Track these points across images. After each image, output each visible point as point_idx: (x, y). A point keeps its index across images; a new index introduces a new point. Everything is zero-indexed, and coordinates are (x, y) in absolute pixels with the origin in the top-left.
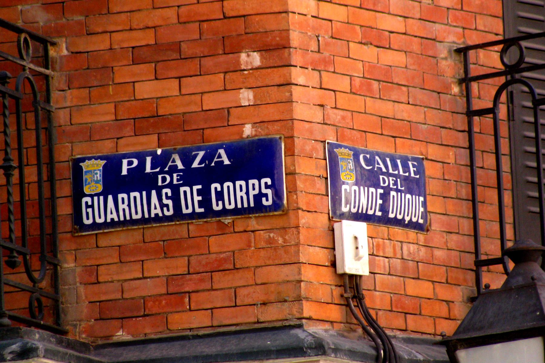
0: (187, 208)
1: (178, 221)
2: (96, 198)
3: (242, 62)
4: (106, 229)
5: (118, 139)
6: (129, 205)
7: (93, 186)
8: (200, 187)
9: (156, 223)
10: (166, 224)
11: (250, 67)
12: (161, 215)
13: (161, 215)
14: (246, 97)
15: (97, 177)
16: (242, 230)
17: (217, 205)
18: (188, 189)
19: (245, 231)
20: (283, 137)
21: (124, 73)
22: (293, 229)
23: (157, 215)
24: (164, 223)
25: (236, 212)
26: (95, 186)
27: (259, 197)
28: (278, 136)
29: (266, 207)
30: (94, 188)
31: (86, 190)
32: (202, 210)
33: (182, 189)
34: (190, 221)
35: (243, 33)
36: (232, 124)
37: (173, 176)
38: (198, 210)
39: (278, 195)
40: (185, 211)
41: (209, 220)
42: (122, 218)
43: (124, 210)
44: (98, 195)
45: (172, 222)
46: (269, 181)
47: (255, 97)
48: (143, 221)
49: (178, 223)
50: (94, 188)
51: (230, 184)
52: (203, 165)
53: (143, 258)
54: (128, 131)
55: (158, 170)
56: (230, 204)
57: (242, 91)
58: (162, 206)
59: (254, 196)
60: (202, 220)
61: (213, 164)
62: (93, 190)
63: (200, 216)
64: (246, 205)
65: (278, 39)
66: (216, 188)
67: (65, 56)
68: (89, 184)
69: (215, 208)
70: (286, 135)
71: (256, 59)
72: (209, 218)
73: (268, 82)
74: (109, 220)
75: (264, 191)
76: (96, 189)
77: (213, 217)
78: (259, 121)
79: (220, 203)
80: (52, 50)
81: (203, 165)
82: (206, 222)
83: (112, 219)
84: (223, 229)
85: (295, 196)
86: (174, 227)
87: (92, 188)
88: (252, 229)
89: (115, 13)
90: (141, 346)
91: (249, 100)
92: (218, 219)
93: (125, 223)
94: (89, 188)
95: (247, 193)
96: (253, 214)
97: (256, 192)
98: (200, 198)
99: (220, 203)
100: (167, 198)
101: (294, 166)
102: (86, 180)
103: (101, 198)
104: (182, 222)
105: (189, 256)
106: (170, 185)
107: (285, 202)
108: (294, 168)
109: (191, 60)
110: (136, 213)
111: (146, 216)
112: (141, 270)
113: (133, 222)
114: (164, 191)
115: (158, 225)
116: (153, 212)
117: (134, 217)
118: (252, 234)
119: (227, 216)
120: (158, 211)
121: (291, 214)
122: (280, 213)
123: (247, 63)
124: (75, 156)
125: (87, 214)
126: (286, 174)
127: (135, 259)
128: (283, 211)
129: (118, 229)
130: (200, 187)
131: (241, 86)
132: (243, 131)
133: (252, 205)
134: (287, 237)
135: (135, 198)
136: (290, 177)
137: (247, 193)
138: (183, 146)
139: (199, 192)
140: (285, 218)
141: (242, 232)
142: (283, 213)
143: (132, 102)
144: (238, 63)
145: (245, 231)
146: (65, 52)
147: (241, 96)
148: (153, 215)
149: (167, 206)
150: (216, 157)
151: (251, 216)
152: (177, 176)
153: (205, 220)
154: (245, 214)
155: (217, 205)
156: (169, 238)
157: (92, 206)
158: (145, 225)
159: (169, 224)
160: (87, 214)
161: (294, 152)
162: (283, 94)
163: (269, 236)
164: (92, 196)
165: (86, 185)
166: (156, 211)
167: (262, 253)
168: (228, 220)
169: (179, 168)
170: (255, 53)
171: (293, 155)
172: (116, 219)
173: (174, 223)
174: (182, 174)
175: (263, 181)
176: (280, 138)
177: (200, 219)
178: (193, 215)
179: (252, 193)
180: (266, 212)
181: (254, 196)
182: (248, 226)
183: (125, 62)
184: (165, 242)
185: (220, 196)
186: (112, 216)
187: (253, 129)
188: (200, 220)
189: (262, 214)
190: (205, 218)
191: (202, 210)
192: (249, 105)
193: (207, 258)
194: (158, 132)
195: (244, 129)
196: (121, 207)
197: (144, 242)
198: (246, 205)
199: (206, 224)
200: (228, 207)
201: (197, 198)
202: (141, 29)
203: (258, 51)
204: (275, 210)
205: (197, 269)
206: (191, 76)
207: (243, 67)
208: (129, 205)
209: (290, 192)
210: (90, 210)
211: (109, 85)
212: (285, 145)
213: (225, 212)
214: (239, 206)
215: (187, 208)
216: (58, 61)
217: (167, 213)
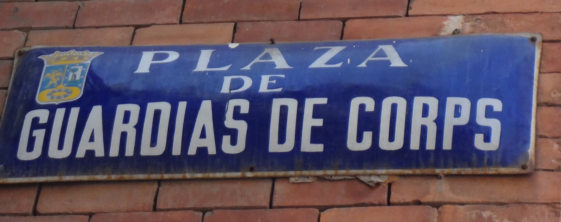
0: (282, 139)
1: (252, 170)
2: (60, 113)
4: (67, 174)
5: (137, 27)
6: (139, 127)
7: (60, 91)
8: (323, 101)
10: (219, 175)
12: (212, 151)
13: (212, 151)
15: (75, 76)
16: (409, 198)
17: (359, 139)
18: (292, 104)
19: (418, 203)
20: (539, 38)
22: (544, 207)
23: (202, 151)
24: (214, 171)
25: (404, 158)
26: (66, 91)
27: (464, 134)
29: (480, 153)
30: (57, 94)
31: (42, 98)
32: (319, 148)
33: (277, 104)
34: (281, 173)
36: (418, 13)
37: (260, 79)
38: (307, 146)
40: (274, 146)
41: (331, 172)
42: (114, 152)
43: (124, 135)
44: (68, 106)
45: (238, 171)
46: (497, 105)
49: (249, 174)
52: (339, 65)
56: (391, 138)
58: (220, 130)
59: (457, 129)
60: (313, 173)
61: (363, 65)
62: (59, 98)
63: (312, 161)
64: (431, 145)
68: (52, 86)
69: (352, 144)
72: (330, 168)
74: (80, 154)
75: (482, 120)
76: (65, 96)
77: (342, 167)
78: (483, 11)
79: (368, 136)
81: (339, 65)
82: (320, 178)
86: (237, 186)
87: (57, 94)
88: (437, 199)
92: (353, 172)
93: (121, 162)
95: (440, 122)
96: (446, 166)
97: (464, 120)
98: (319, 122)
99: (368, 136)
102: (47, 81)
103: (75, 112)
106: (252, 96)
107: (531, 150)
110: (154, 142)
111: (176, 150)
113: (140, 162)
117: (146, 150)
120: (210, 144)
122: (516, 170)
124: (30, 46)
126: (538, 105)
128: (524, 167)
129: (99, 177)
130: (323, 101)
132: (442, 26)
133: (447, 144)
135: (157, 114)
137: (440, 122)
139: (318, 112)
141: (407, 204)
142: (523, 172)
145: (418, 203)
148: (192, 151)
149: (233, 133)
150: (374, 54)
151: (438, 171)
152: (271, 79)
153: (320, 173)
154: (427, 166)
155: (359, 139)
156: (219, 205)
157: (48, 127)
158: (168, 172)
159: (229, 175)
163: (480, 216)
164: (52, 109)
165: (42, 90)
166: (203, 140)
168: (380, 175)
169: (278, 67)
172: (100, 152)
173: (238, 174)
174: (283, 76)
175: (482, 103)
176: (533, 40)
178: (295, 159)
179: (450, 122)
180: (480, 165)
181: (457, 129)
182: (427, 193)
184: (208, 214)
185: (369, 122)
187: (468, 24)
188: (306, 173)
190: (320, 168)
191: (319, 148)
194: (235, 18)
195: (445, 23)
196: (118, 126)
198: (431, 145)
199: (319, 185)
200: (384, 144)
201: (310, 122)
204: (504, 164)
208: (139, 127)
209: (541, 137)
210: (40, 134)
212: (542, 54)
213: (374, 157)
214: (415, 145)
215: (282, 139)
217: (227, 148)
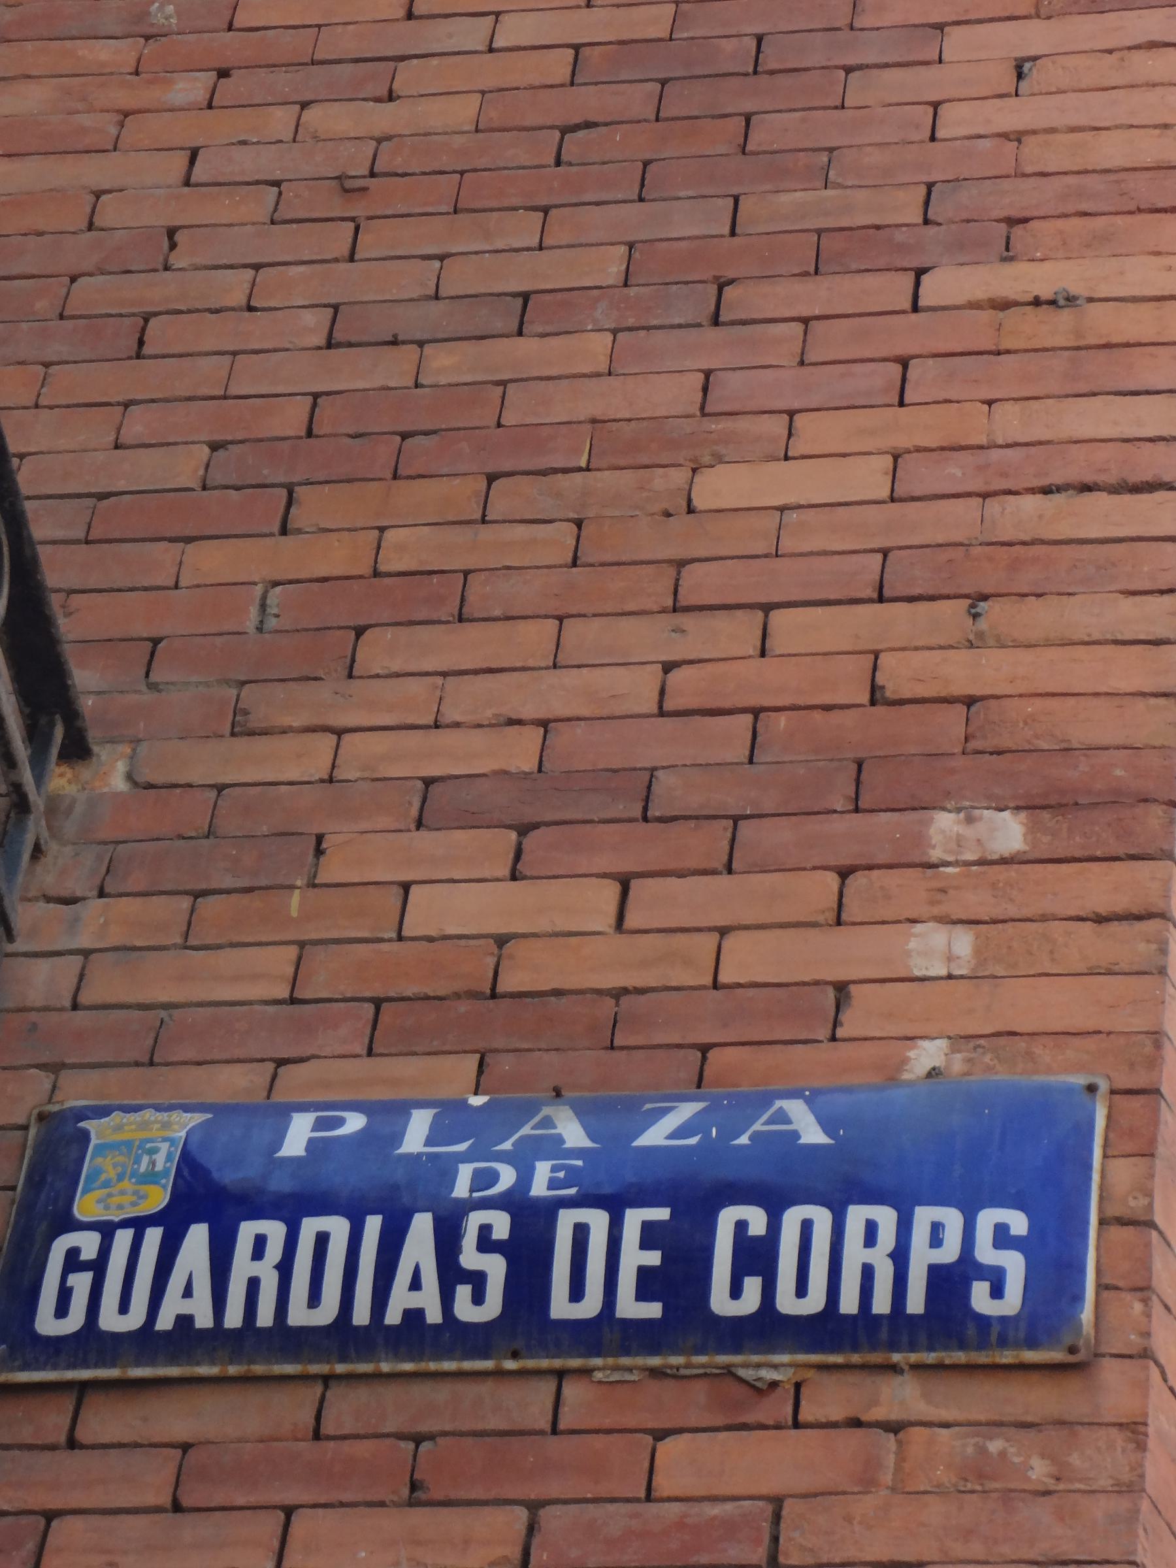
0: (577, 1292)
1: (515, 1355)
2: (123, 1239)
3: (936, 839)
4: (138, 1364)
6: (285, 1268)
7: (123, 1193)
8: (661, 1214)
9: (398, 1357)
10: (449, 1365)
11: (970, 856)
12: (434, 1316)
13: (434, 1316)
14: (938, 949)
15: (154, 1163)
16: (837, 1414)
17: (736, 1291)
21: (366, 854)
22: (1114, 1431)
24: (438, 1357)
25: (826, 1330)
26: (135, 1193)
27: (948, 1283)
28: (1081, 1080)
29: (984, 1321)
31: (86, 1207)
32: (653, 1310)
33: (567, 1220)
34: (575, 1363)
35: (958, 750)
37: (532, 1169)
38: (629, 1307)
39: (1054, 1273)
40: (561, 1307)
41: (676, 1360)
42: (234, 1318)
44: (139, 1225)
45: (486, 1356)
47: (978, 951)
48: (342, 1336)
49: (510, 1365)
50: (126, 1200)
51: (822, 1217)
52: (693, 1141)
53: (290, 1497)
54: (349, 1031)
55: (462, 1147)
57: (918, 928)
60: (640, 1361)
61: (744, 1140)
62: (120, 1207)
63: (639, 1336)
64: (882, 1304)
65: (1119, 772)
66: (741, 1226)
67: (117, 795)
68: (107, 1184)
69: (721, 1303)
70: (1123, 1082)
71: (1008, 832)
73: (1048, 905)
74: (165, 1322)
75: (986, 1253)
76: (134, 1204)
80: (61, 775)
81: (693, 1141)
83: (185, 1321)
84: (740, 1410)
85: (1138, 1307)
86: (485, 1388)
87: (116, 1200)
89: (378, 676)
90: (666, 697)
91: (950, 958)
93: (247, 1340)
94: (99, 1201)
95: (900, 1257)
96: (913, 1348)
97: (949, 1253)
98: (653, 1258)
99: (753, 1286)
100: (486, 1243)
101: (1149, 1194)
102: (96, 1173)
103: (153, 1236)
104: (531, 1363)
105: (534, 1507)
106: (516, 1203)
107: (1087, 1314)
108: (1143, 1201)
109: (692, 824)
110: (314, 1298)
111: (361, 1315)
112: (276, 1544)
113: (287, 1339)
114: (476, 1219)
115: (408, 1367)
116: (400, 1300)
117: (299, 1315)
118: (890, 1440)
119: (772, 1350)
120: (429, 1301)
121: (1111, 1373)
123: (959, 841)
124: (62, 1102)
125: (65, 1295)
126: (1102, 1222)
127: (253, 1499)
128: (1072, 1350)
129: (204, 1370)
130: (661, 1214)
131: (924, 911)
132: (905, 1060)
133: (916, 1303)
134: (1075, 1460)
135: (322, 1240)
136: (1117, 1233)
137: (900, 1257)
138: (595, 1094)
140: (1073, 1383)
142: (1071, 1359)
143: (385, 947)
144: (920, 839)
145: (856, 1423)
146: (118, 783)
147: (913, 944)
148: (393, 1317)
149: (478, 1280)
151: (896, 1357)
152: (554, 1169)
153: (655, 1361)
155: (736, 1291)
157: (98, 1267)
158: (343, 1359)
160: (65, 1295)
161: (1152, 1141)
162: (1125, 946)
163: (982, 1451)
164: (107, 1231)
165: (84, 1192)
166: (416, 1295)
167: (935, 1511)
168: (778, 1365)
170: (1006, 814)
171: (1148, 1154)
172: (204, 1320)
173: (488, 1364)
174: (580, 1163)
176: (1092, 1089)
177: (627, 1352)
178: (604, 1333)
179: (921, 1257)
182: (875, 1402)
183: (384, 822)
184: (425, 1446)
185: (756, 1257)
186: (189, 1301)
188: (625, 1361)
189: (960, 1357)
190: (654, 1350)
191: (653, 1310)
192: (950, 977)
193: (636, 1515)
195: (911, 1054)
196: (242, 1266)
197: (704, 415)
198: (882, 1304)
199: (654, 1386)
200: (787, 1303)
202: (479, 726)
203: (1018, 808)
204: (1032, 1343)
205: (574, 1553)
206: (681, 874)
207: (936, 855)
208: (285, 1268)
210: (81, 1282)
211: (292, 887)
213: (767, 1327)
214: (849, 1304)
215: (577, 1292)
216: (79, 809)
217: (465, 1310)
